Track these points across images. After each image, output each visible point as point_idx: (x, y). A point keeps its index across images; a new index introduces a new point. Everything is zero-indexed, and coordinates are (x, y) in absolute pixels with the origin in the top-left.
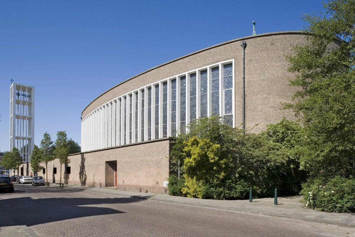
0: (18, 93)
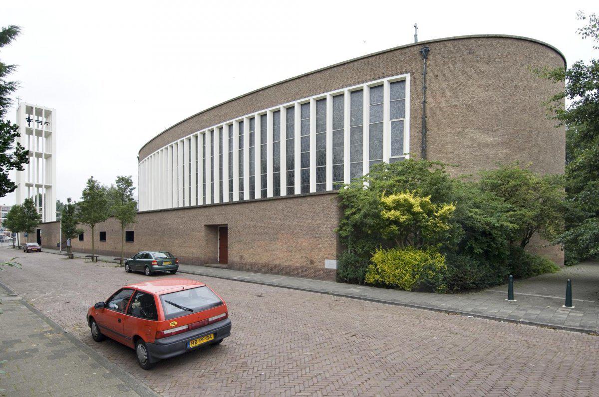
0: (29, 117)
